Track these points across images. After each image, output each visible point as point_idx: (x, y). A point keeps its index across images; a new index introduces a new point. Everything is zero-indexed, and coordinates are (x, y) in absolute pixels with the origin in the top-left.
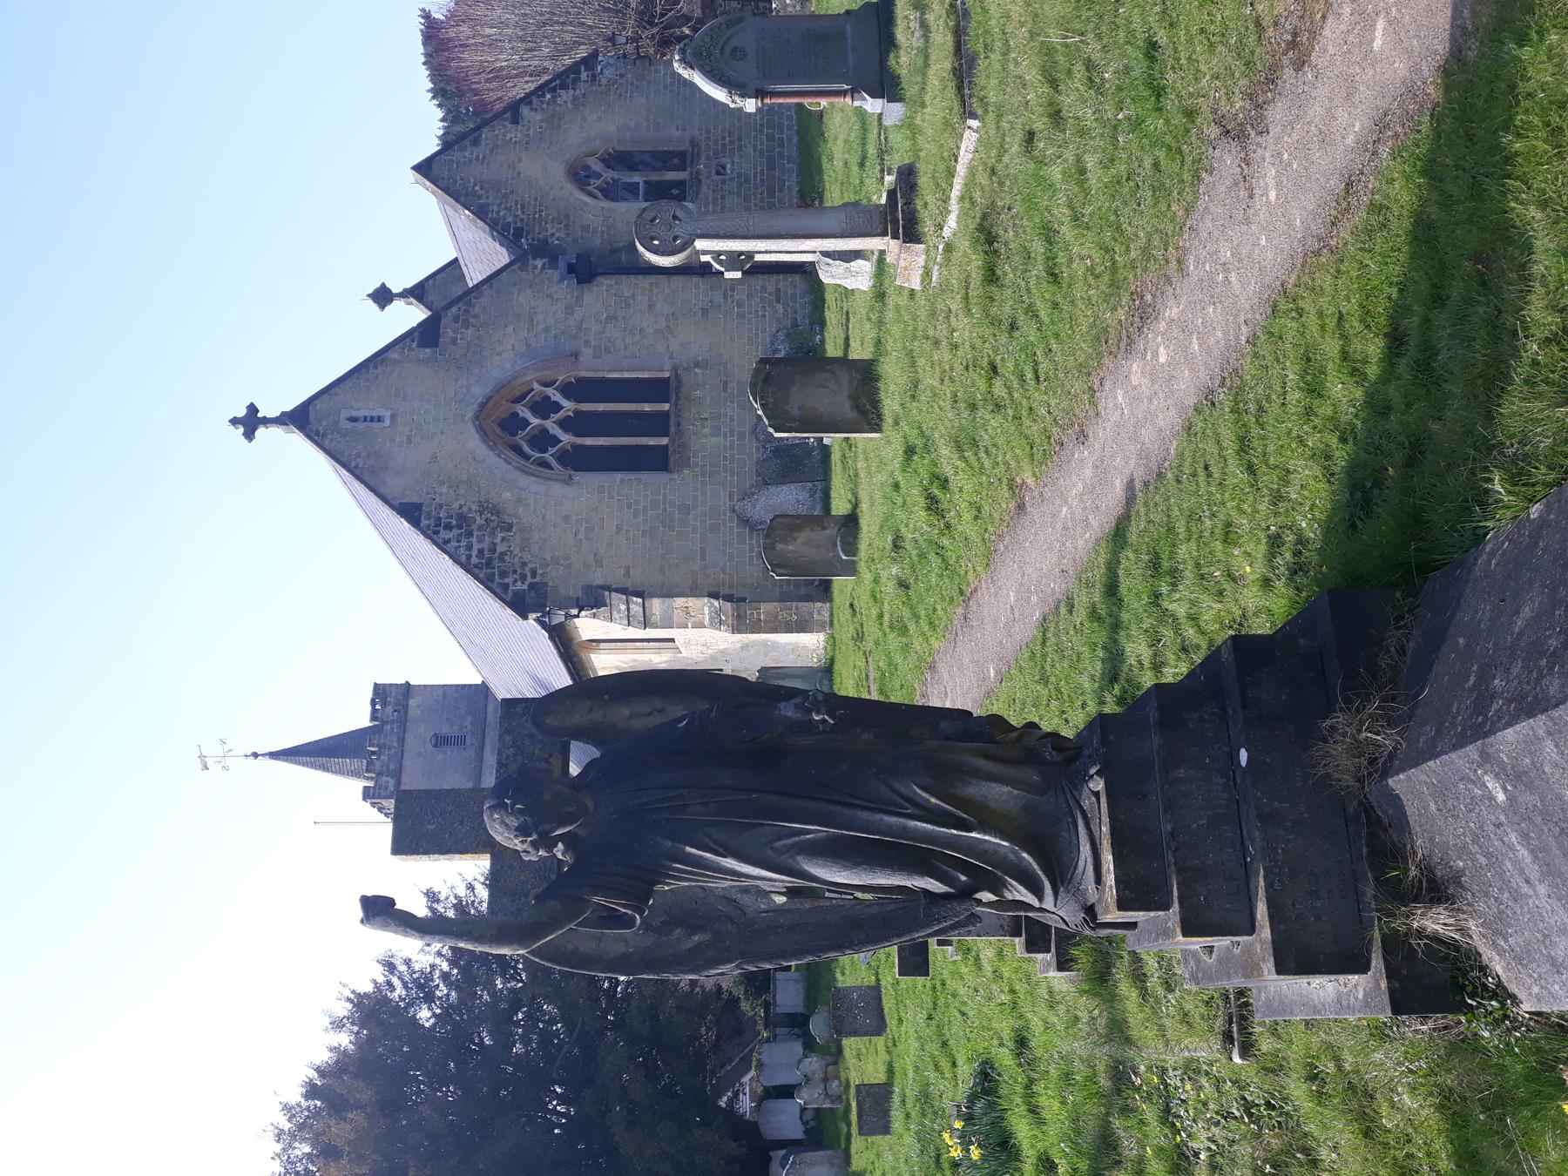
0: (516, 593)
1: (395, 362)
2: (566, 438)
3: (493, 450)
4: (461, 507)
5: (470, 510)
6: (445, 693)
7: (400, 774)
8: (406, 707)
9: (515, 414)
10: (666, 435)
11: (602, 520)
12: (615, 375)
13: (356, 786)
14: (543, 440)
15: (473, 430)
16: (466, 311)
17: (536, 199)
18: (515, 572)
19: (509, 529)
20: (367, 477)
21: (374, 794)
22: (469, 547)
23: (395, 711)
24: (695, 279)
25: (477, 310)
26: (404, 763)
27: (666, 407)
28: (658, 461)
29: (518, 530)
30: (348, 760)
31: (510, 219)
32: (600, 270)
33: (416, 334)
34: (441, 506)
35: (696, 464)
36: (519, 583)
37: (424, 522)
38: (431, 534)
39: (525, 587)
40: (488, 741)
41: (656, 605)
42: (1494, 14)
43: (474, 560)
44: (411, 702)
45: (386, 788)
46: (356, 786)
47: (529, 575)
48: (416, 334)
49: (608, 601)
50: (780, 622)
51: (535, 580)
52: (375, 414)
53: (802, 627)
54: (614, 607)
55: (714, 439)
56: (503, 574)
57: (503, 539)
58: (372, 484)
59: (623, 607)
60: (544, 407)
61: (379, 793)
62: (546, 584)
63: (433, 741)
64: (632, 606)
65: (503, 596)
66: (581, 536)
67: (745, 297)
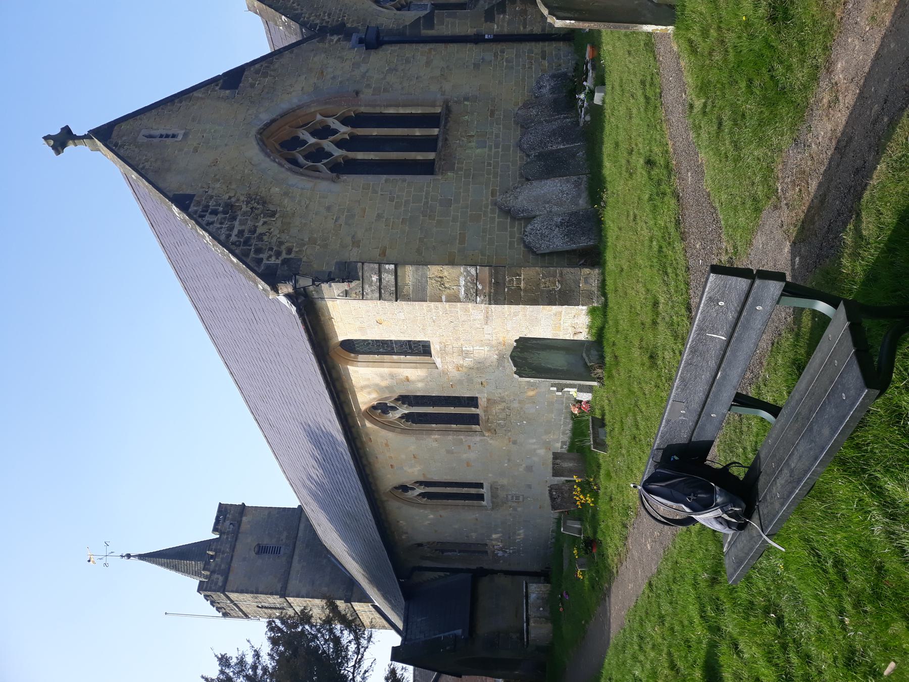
0: (268, 267)
1: (198, 98)
2: (338, 153)
3: (269, 156)
4: (230, 198)
5: (238, 200)
6: (269, 513)
7: (228, 573)
8: (240, 523)
9: (297, 138)
10: (434, 150)
11: (364, 210)
12: (391, 111)
13: (195, 582)
14: (318, 154)
15: (255, 143)
16: (266, 67)
17: (341, 10)
18: (271, 249)
19: (273, 214)
20: (150, 175)
21: (206, 587)
22: (231, 229)
23: (231, 524)
24: (469, 46)
25: (276, 66)
26: (232, 565)
27: (435, 131)
28: (427, 168)
29: (280, 216)
30: (193, 562)
31: (318, 21)
32: (386, 39)
33: (221, 81)
34: (212, 197)
35: (460, 169)
36: (273, 258)
37: (192, 208)
38: (199, 218)
39: (279, 262)
40: (297, 552)
41: (409, 274)
42: (792, 357)
43: (233, 238)
44: (244, 519)
45: (216, 583)
46: (195, 582)
47: (284, 252)
48: (221, 81)
49: (360, 274)
50: (542, 291)
51: (290, 256)
52: (170, 133)
53: (565, 298)
54: (366, 281)
55: (478, 151)
56: (258, 251)
57: (265, 223)
58: (153, 181)
59: (375, 278)
60: (324, 132)
61: (211, 588)
62: (300, 260)
63: (256, 550)
64: (384, 276)
65: (256, 268)
66: (342, 220)
67: (514, 56)
